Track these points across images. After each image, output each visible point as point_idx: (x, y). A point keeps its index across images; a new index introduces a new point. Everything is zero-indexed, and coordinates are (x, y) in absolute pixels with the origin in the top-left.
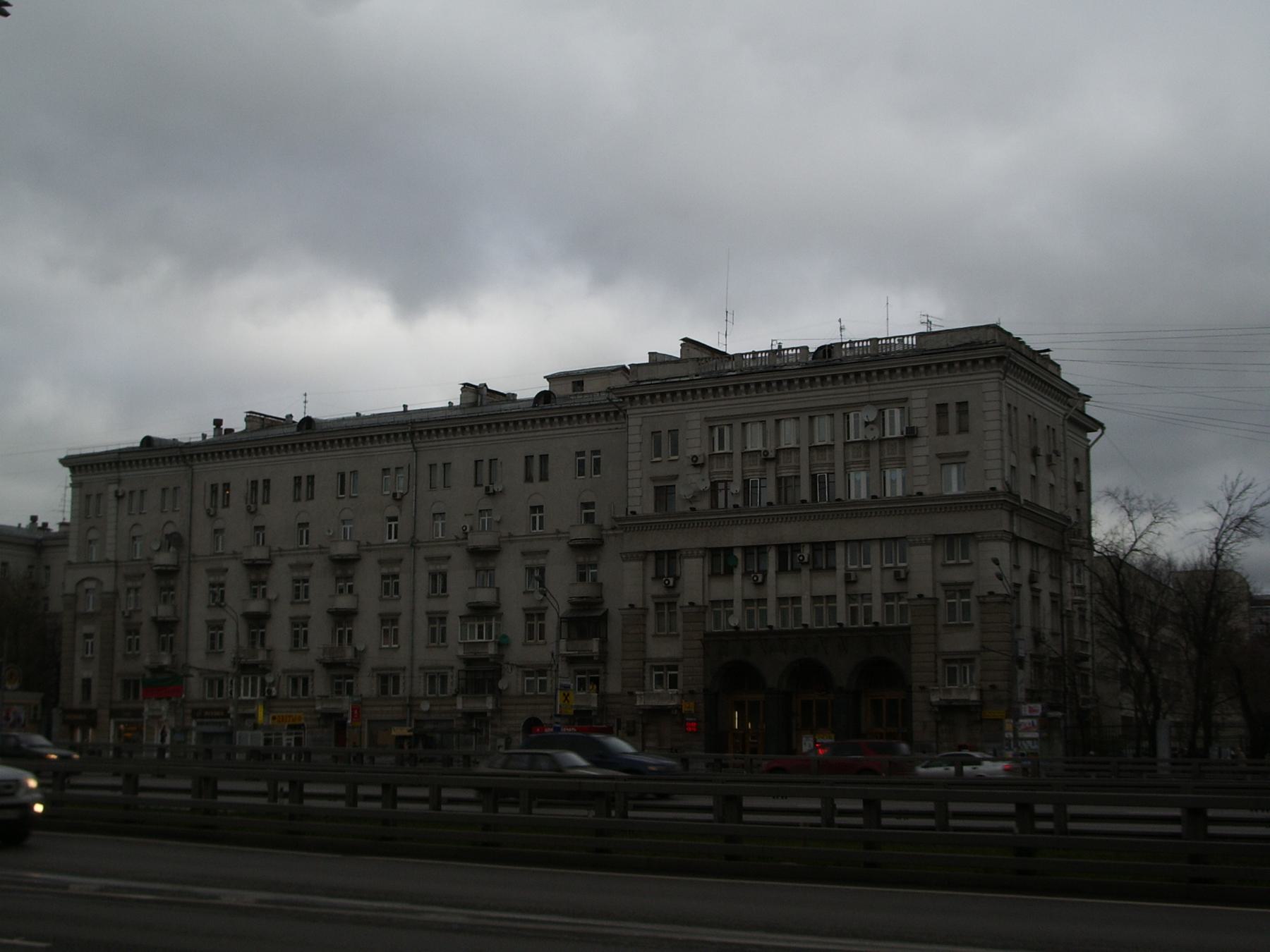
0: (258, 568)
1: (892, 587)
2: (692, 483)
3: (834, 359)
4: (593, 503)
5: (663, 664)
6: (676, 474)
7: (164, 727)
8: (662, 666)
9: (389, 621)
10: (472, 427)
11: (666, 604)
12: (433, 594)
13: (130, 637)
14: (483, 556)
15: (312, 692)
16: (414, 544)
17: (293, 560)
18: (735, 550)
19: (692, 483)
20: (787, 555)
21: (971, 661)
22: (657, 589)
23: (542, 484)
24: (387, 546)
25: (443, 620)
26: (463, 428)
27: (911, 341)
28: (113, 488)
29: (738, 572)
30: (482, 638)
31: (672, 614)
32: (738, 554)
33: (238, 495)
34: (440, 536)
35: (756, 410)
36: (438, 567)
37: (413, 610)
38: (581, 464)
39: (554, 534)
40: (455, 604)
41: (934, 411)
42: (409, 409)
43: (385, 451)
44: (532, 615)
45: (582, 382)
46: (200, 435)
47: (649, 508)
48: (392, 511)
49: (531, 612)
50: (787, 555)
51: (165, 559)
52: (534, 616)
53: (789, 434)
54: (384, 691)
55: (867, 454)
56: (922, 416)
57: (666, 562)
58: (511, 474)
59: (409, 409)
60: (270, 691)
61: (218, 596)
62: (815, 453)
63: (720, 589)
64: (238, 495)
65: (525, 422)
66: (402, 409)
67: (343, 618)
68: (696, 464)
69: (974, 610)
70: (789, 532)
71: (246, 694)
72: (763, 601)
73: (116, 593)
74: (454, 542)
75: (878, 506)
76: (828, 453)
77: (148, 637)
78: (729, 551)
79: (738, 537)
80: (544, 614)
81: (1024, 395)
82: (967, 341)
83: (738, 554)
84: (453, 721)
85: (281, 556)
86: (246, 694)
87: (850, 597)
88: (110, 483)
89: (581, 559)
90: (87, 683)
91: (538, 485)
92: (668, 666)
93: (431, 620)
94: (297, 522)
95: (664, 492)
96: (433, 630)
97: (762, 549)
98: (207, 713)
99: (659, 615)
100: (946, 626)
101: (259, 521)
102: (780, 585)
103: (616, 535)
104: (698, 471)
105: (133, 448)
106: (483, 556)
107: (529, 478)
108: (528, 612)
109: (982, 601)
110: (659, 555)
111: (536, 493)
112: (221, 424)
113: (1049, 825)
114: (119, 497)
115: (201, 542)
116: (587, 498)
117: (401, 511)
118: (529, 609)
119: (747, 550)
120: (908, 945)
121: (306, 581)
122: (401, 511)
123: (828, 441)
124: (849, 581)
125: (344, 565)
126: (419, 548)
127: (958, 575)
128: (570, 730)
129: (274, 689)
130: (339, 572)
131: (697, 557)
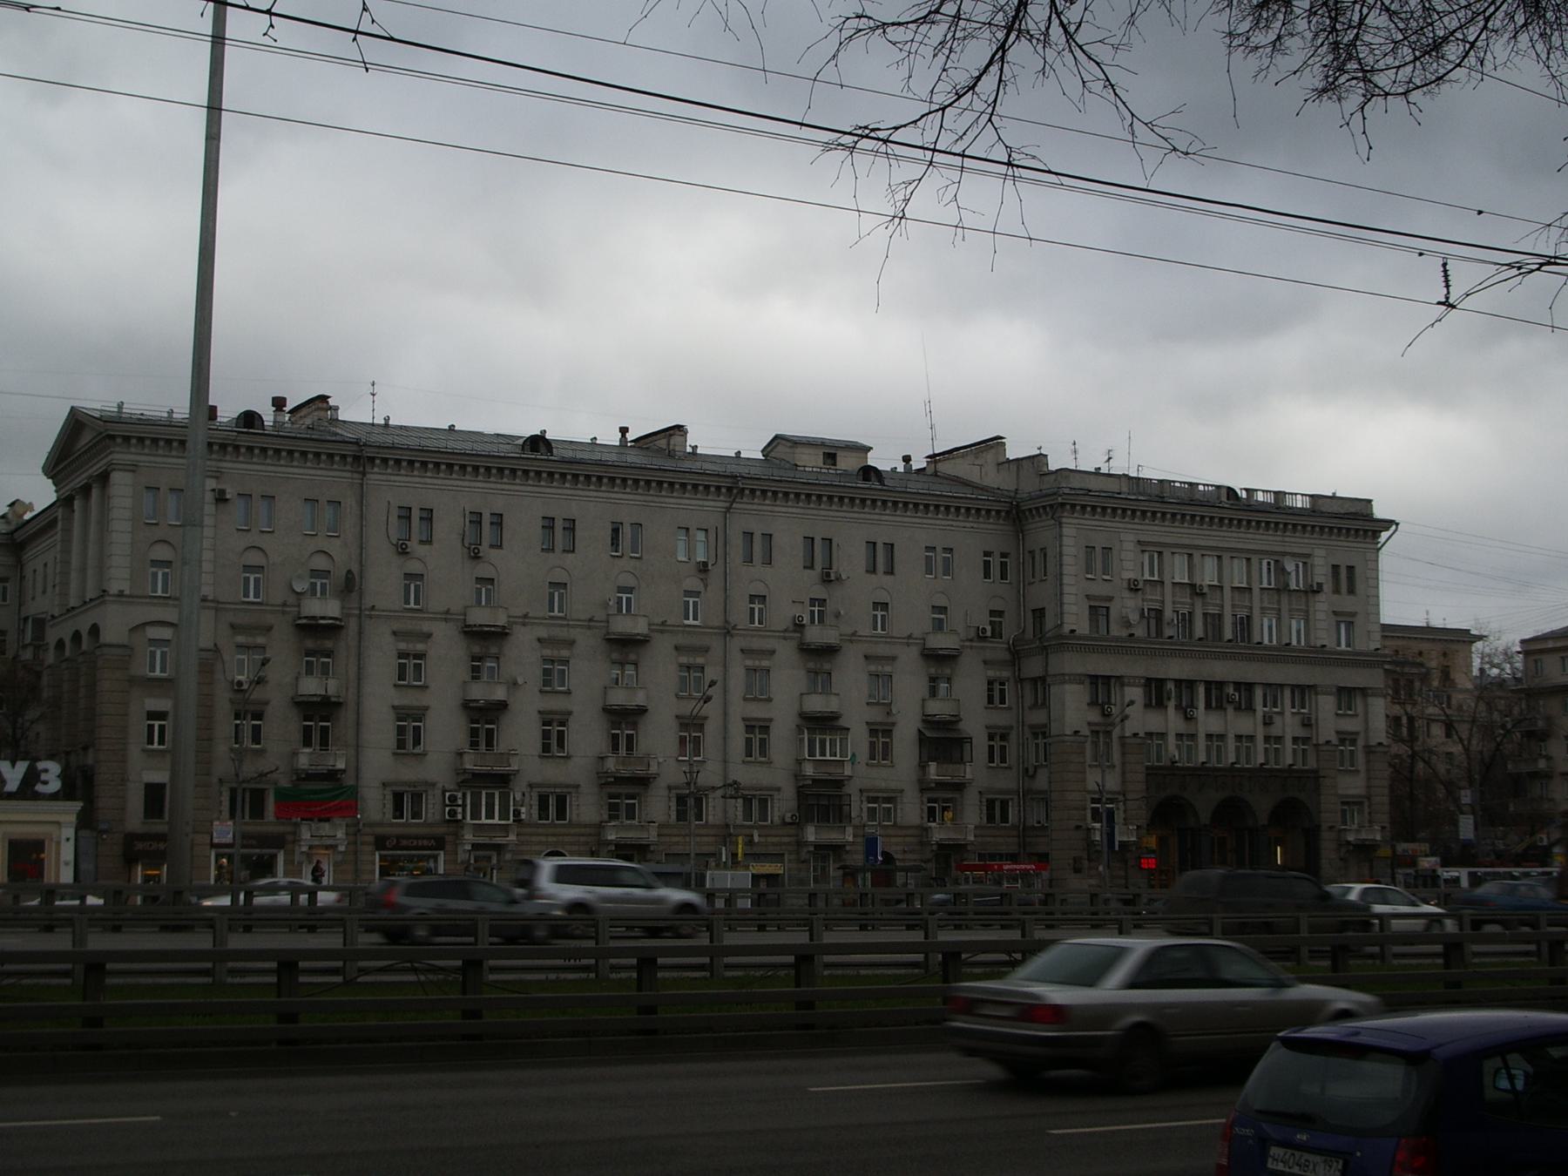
0: (940, 661)
1: (1301, 733)
2: (1127, 606)
4: (1003, 612)
5: (880, 795)
6: (1111, 595)
7: (318, 862)
8: (878, 798)
9: (691, 726)
10: (636, 481)
11: (1100, 732)
12: (415, 683)
13: (238, 722)
14: (819, 656)
15: (578, 815)
16: (727, 631)
17: (543, 633)
18: (1168, 682)
19: (1127, 606)
20: (1218, 695)
21: (1360, 804)
22: (1094, 716)
23: (889, 578)
24: (687, 629)
25: (765, 729)
26: (830, 498)
27: (1299, 503)
28: (211, 484)
29: (1172, 704)
30: (825, 755)
31: (1108, 745)
32: (1171, 686)
33: (449, 527)
34: (879, 630)
35: (1187, 542)
36: (880, 668)
37: (725, 714)
38: (987, 564)
39: (279, 606)
40: (782, 713)
41: (1330, 570)
42: (699, 451)
43: (395, 481)
44: (877, 731)
45: (835, 454)
46: (116, 405)
47: (1083, 628)
48: (693, 583)
49: (753, 723)
50: (1218, 695)
51: (326, 608)
52: (881, 732)
53: (1208, 574)
54: (681, 815)
55: (1279, 602)
56: (1321, 574)
57: (1101, 687)
58: (851, 560)
59: (699, 451)
60: (517, 813)
61: (410, 666)
62: (1236, 594)
63: (1154, 722)
64: (449, 527)
65: (947, 508)
66: (383, 422)
67: (624, 719)
68: (1133, 587)
69: (1360, 758)
70: (1220, 670)
71: (490, 815)
72: (1193, 737)
73: (216, 650)
74: (586, 623)
75: (1283, 654)
76: (1159, 588)
77: (281, 728)
78: (1161, 682)
79: (1175, 669)
80: (768, 727)
82: (1353, 510)
83: (1171, 686)
84: (783, 854)
85: (524, 624)
86: (490, 815)
87: (1267, 739)
88: (208, 477)
89: (933, 671)
90: (154, 793)
91: (881, 578)
92: (884, 798)
93: (750, 728)
94: (475, 576)
95: (1098, 610)
96: (991, 748)
97: (1191, 684)
98: (404, 842)
99: (1095, 744)
100: (1090, 766)
101: (484, 571)
102: (1208, 722)
103: (971, 647)
104: (1132, 595)
106: (819, 656)
107: (872, 570)
108: (748, 723)
109: (1369, 750)
110: (1094, 680)
111: (165, 541)
112: (285, 406)
114: (221, 498)
115: (383, 584)
116: (941, 601)
117: (706, 586)
118: (872, 724)
119: (1178, 682)
121: (566, 662)
122: (706, 586)
124: (1268, 722)
125: (626, 647)
126: (732, 636)
127: (1350, 725)
129: (523, 810)
130: (615, 656)
131: (1137, 686)
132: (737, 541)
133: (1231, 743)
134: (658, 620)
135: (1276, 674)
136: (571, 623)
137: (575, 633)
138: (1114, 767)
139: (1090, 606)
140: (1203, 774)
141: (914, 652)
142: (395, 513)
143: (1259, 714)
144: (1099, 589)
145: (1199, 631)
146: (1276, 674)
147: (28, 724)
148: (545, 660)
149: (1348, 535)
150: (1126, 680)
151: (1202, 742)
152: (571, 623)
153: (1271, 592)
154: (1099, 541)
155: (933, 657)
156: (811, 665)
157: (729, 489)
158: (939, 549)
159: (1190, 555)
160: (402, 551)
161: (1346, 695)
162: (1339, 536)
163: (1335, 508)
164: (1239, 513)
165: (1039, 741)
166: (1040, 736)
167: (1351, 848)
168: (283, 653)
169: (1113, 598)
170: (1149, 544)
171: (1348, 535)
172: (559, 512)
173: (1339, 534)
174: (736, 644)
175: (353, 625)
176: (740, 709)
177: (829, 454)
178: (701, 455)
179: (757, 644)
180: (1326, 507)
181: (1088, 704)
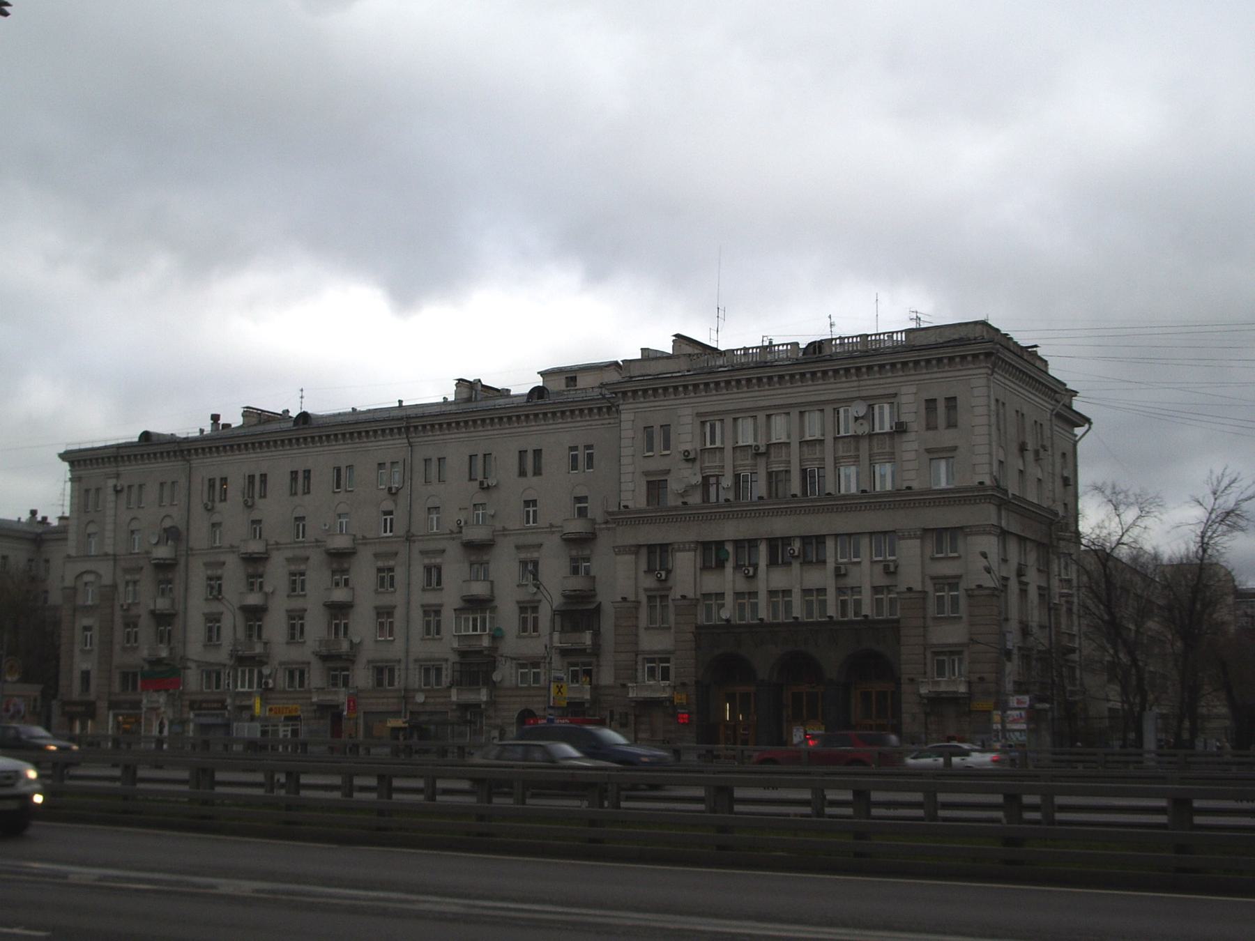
1: (882, 581)
2: (684, 477)
3: (824, 354)
5: (656, 656)
7: (162, 718)
8: (654, 658)
9: (384, 613)
11: (658, 597)
14: (477, 550)
16: (409, 538)
17: (289, 554)
19: (684, 477)
20: (778, 549)
21: (960, 653)
22: (649, 582)
26: (475, 422)
27: (901, 337)
29: (729, 566)
30: (477, 631)
31: (665, 607)
32: (730, 548)
33: (235, 489)
34: (435, 530)
35: (748, 405)
37: (408, 603)
38: (575, 458)
42: (404, 404)
44: (526, 608)
46: (198, 430)
47: (641, 502)
49: (525, 605)
50: (778, 549)
51: (163, 552)
52: (528, 608)
54: (379, 683)
55: (857, 449)
59: (404, 404)
61: (215, 589)
63: (711, 582)
64: (235, 489)
67: (339, 611)
68: (688, 458)
70: (780, 526)
71: (243, 686)
72: (754, 594)
73: (114, 586)
75: (868, 500)
78: (720, 544)
79: (729, 531)
81: (769, 398)
82: (956, 337)
83: (730, 548)
86: (243, 686)
87: (840, 591)
89: (574, 553)
91: (532, 480)
93: (426, 613)
94: (294, 516)
95: (656, 487)
97: (753, 543)
98: (204, 705)
99: (652, 608)
102: (770, 579)
103: (608, 529)
105: (132, 443)
106: (477, 550)
107: (522, 473)
109: (970, 595)
110: (651, 548)
112: (219, 420)
113: (1036, 816)
115: (199, 536)
116: (581, 492)
117: (396, 505)
119: (738, 543)
120: (897, 934)
121: (302, 574)
122: (396, 505)
123: (784, 439)
124: (839, 574)
125: (340, 559)
128: (265, 761)
132: (419, 467)
133: (796, 599)
134: (359, 536)
135: (843, 523)
136: (306, 545)
137: (222, 558)
138: (670, 628)
139: (648, 482)
140: (762, 631)
141: (556, 539)
142: (206, 482)
143: (831, 564)
144: (655, 465)
145: (795, 487)
146: (843, 523)
147: (1085, 579)
148: (380, 570)
149: (162, 456)
150: (676, 547)
151: (762, 599)
152: (306, 545)
153: (848, 440)
154: (657, 420)
155: (473, 547)
156: (473, 558)
157: (407, 428)
158: (581, 448)
159: (755, 417)
160: (209, 510)
161: (945, 537)
162: (104, 464)
163: (932, 339)
164: (809, 366)
165: (432, 619)
166: (529, 611)
167: (925, 701)
168: (147, 582)
169: (670, 470)
170: (705, 414)
171: (149, 458)
172: (300, 466)
173: (149, 458)
174: (417, 547)
175: (182, 561)
176: (420, 598)
177: (571, 377)
178: (405, 406)
179: (432, 546)
180: (921, 340)
181: (645, 572)
